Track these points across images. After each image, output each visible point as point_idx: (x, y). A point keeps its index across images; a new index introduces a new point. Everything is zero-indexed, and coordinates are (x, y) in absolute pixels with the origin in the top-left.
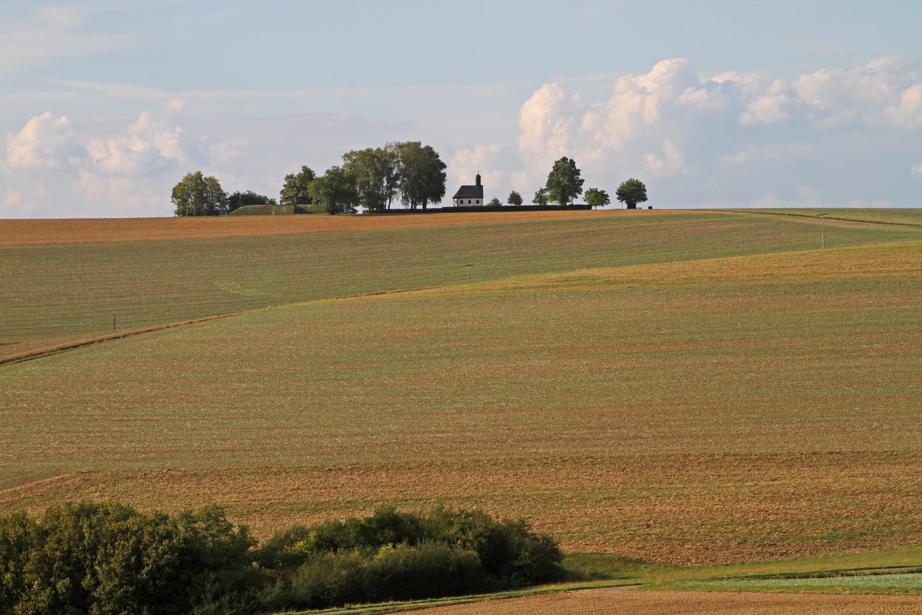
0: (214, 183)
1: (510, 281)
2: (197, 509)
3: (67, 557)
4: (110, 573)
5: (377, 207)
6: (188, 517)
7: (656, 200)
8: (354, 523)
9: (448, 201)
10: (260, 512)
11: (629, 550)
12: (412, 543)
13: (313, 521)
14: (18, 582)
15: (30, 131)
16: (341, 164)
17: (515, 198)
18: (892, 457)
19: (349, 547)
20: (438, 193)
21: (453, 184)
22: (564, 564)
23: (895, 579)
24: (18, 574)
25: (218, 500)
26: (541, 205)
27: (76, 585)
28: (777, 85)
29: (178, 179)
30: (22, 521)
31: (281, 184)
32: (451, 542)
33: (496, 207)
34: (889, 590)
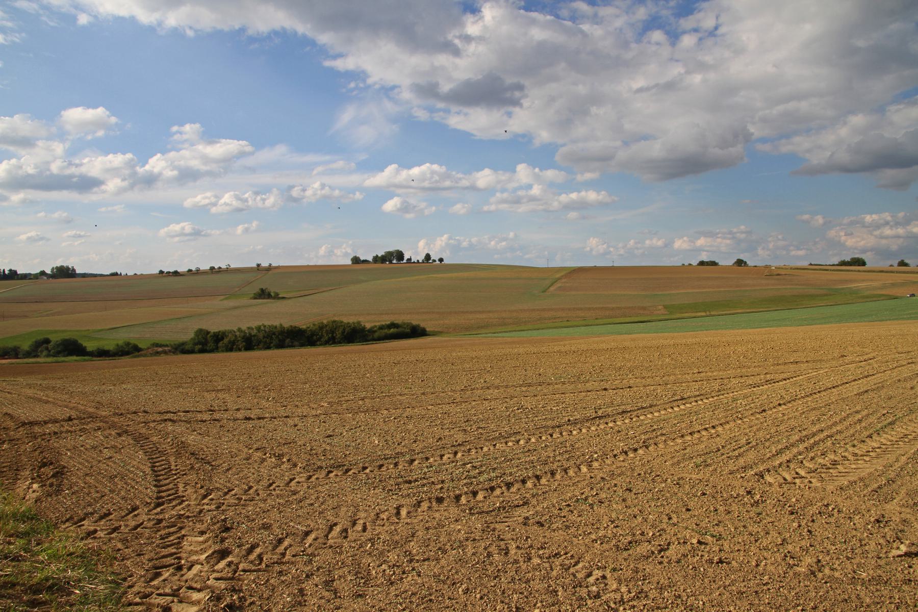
0: (359, 258)
1: (417, 277)
2: (355, 321)
3: (331, 330)
4: (339, 333)
5: (391, 262)
6: (354, 323)
7: (446, 262)
8: (386, 324)
9: (405, 261)
10: (368, 322)
11: (440, 330)
12: (397, 328)
13: (378, 324)
14: (322, 335)
15: (323, 248)
16: (384, 254)
17: (418, 261)
18: (489, 312)
19: (385, 329)
20: (403, 259)
21: (406, 257)
22: (427, 333)
23: (490, 335)
24: (322, 333)
25: (360, 320)
26: (423, 262)
27: (332, 336)
28: (467, 240)
29: (352, 257)
30: (322, 323)
31: (372, 258)
32: (405, 328)
33: (414, 262)
34: (489, 337)
